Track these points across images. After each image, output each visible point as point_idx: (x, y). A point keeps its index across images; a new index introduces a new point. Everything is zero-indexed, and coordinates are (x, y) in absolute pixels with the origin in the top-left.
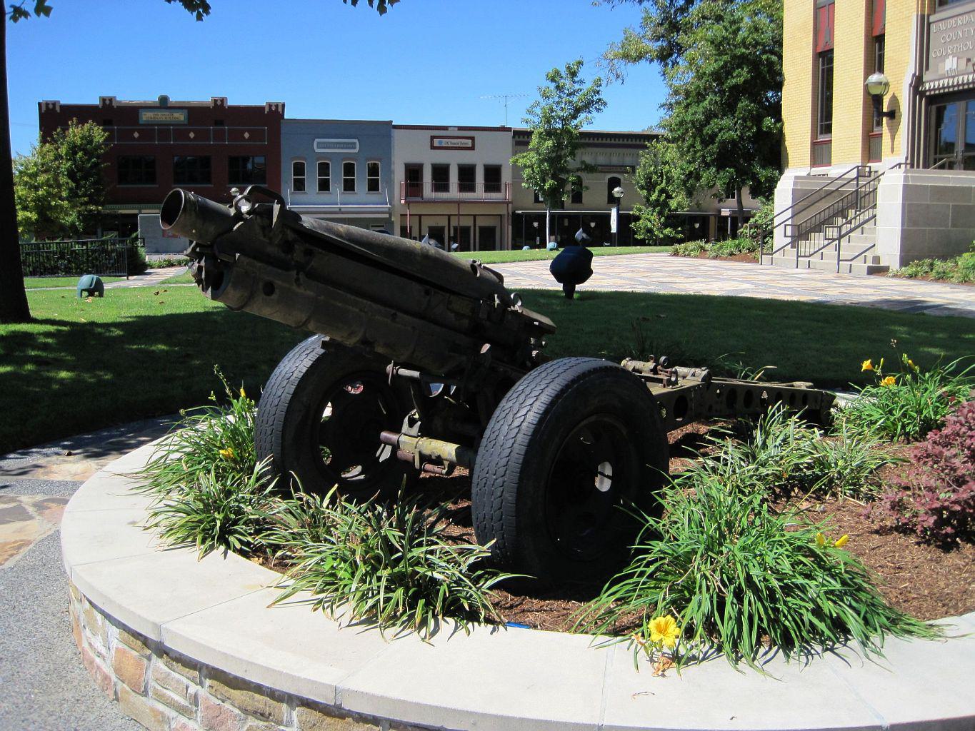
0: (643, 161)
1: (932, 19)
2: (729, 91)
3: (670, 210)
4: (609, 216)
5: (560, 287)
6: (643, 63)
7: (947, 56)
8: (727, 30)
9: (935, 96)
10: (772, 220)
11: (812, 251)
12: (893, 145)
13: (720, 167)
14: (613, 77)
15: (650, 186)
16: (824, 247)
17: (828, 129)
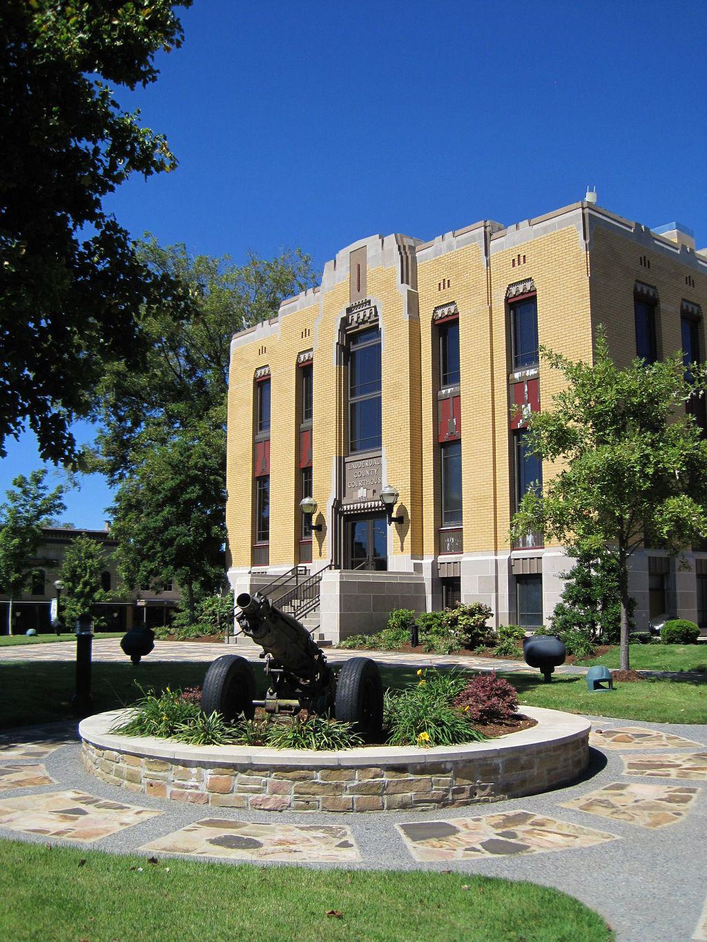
0: (68, 555)
1: (347, 460)
3: (94, 601)
4: (48, 607)
6: (98, 475)
7: (359, 487)
8: (182, 455)
10: (233, 610)
12: (320, 550)
13: (177, 566)
14: (71, 485)
17: (265, 537)
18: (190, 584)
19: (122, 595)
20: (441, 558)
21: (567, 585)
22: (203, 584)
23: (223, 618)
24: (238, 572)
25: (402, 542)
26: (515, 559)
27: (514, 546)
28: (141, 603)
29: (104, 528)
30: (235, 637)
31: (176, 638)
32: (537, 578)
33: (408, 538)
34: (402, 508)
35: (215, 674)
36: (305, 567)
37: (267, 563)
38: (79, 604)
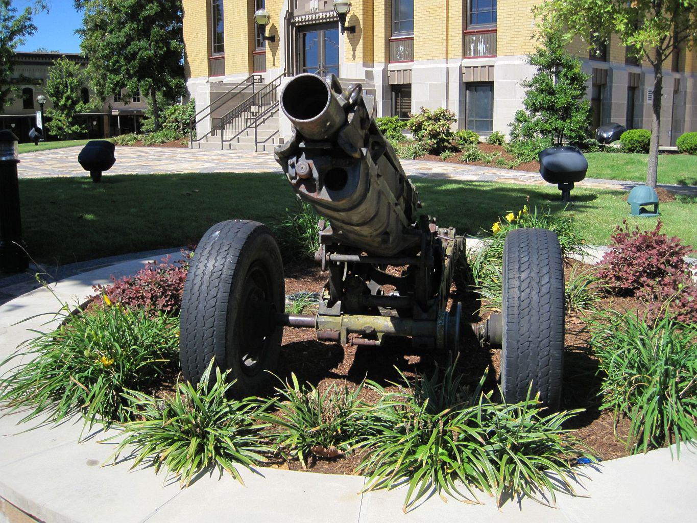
0: (51, 74)
2: (144, 20)
3: (75, 112)
5: (88, 174)
9: (303, 26)
11: (232, 137)
12: (274, 60)
14: (40, 8)
15: (58, 93)
16: (239, 133)
18: (153, 95)
19: (95, 106)
20: (392, 66)
21: (528, 93)
22: (165, 95)
23: (186, 125)
24: (197, 82)
25: (354, 51)
26: (466, 67)
27: (465, 55)
28: (115, 112)
29: (79, 51)
30: (198, 142)
31: (143, 144)
32: (489, 86)
33: (360, 47)
34: (354, 17)
35: (208, 272)
36: (261, 76)
37: (223, 74)
38: (64, 115)
